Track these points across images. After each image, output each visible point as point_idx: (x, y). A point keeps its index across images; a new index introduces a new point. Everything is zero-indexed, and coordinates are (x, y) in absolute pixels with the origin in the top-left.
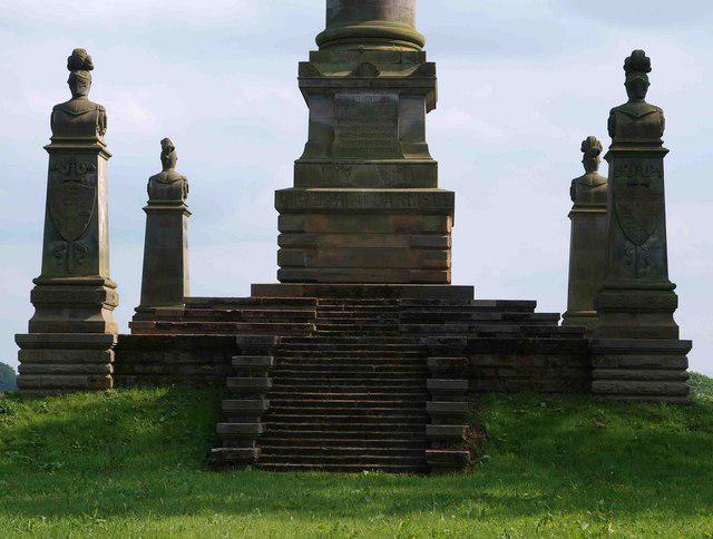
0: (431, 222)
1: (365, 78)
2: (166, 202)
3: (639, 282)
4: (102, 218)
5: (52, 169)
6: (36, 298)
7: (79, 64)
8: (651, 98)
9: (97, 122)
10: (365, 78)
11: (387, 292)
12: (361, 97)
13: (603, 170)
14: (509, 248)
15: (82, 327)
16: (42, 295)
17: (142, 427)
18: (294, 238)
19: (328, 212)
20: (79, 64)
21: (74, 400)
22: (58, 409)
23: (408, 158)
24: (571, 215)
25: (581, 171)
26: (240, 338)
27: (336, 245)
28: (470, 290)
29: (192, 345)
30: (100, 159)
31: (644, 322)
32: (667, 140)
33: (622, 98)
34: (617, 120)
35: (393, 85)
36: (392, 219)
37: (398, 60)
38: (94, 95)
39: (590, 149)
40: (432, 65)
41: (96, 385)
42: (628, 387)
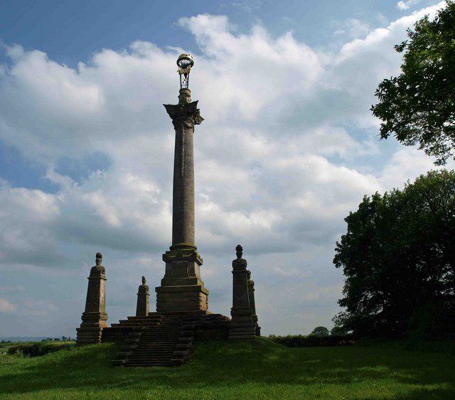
1: (179, 258)
4: (102, 295)
5: (89, 283)
6: (83, 318)
9: (244, 264)
10: (179, 258)
11: (183, 313)
12: (178, 262)
14: (219, 303)
15: (93, 326)
16: (85, 317)
17: (102, 356)
19: (169, 292)
21: (89, 347)
22: (83, 350)
23: (190, 277)
28: (402, 66)
30: (102, 281)
35: (186, 259)
37: (188, 252)
38: (103, 264)
41: (96, 341)
42: (243, 218)
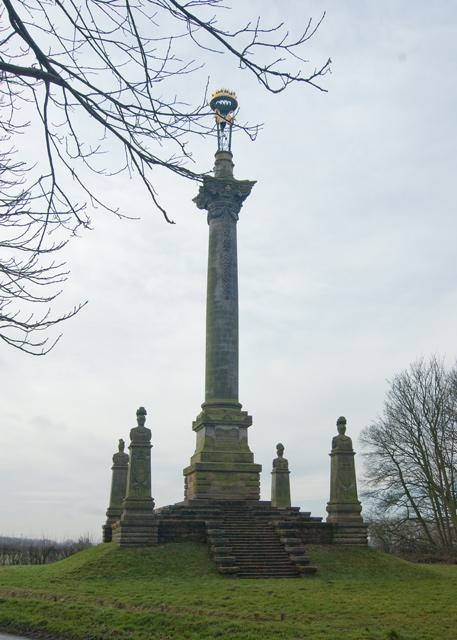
0: (254, 476)
2: (281, 469)
3: (349, 501)
7: (141, 413)
8: (146, 425)
9: (147, 434)
13: (127, 451)
18: (202, 482)
20: (141, 413)
24: (113, 468)
25: (277, 457)
26: (207, 522)
27: (217, 483)
29: (176, 526)
31: (352, 516)
32: (152, 441)
33: (136, 425)
34: (134, 434)
36: (239, 475)
39: (122, 445)
40: (251, 417)
